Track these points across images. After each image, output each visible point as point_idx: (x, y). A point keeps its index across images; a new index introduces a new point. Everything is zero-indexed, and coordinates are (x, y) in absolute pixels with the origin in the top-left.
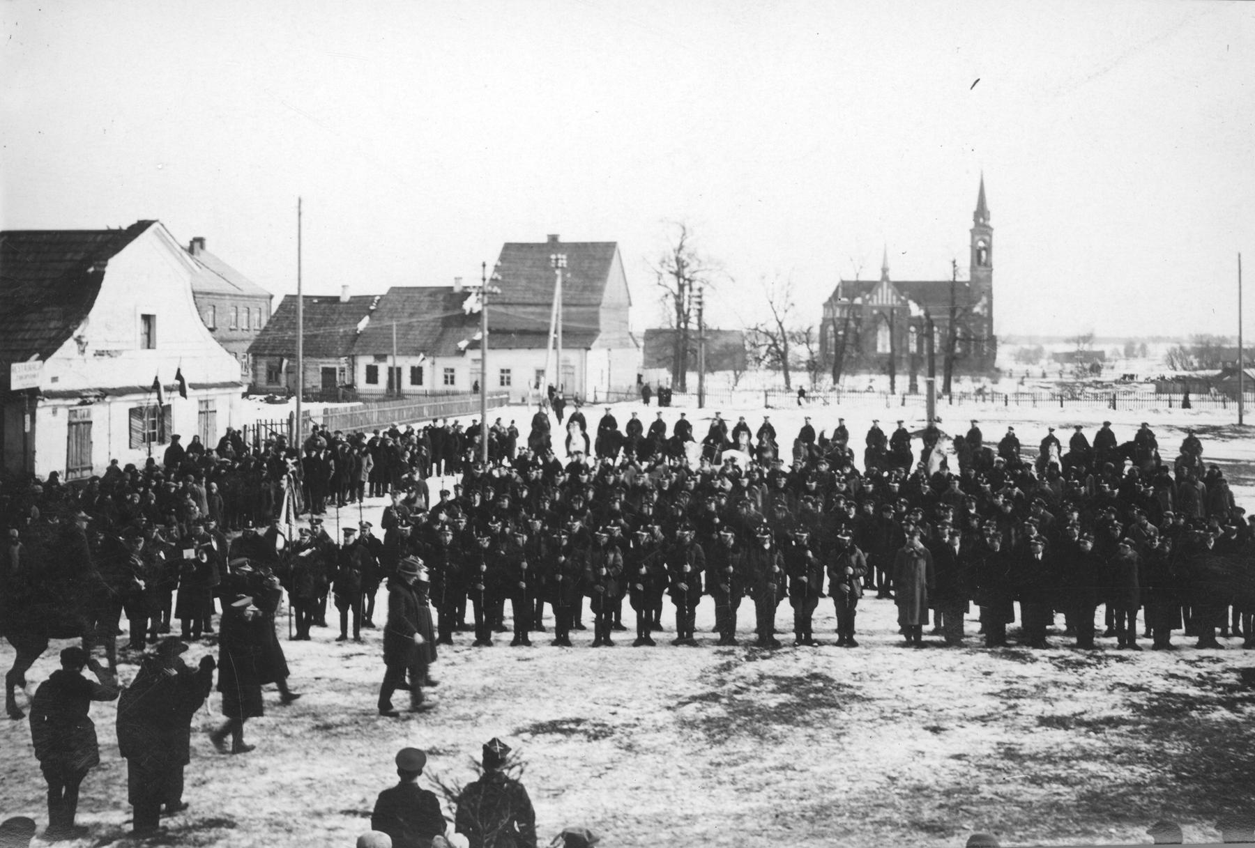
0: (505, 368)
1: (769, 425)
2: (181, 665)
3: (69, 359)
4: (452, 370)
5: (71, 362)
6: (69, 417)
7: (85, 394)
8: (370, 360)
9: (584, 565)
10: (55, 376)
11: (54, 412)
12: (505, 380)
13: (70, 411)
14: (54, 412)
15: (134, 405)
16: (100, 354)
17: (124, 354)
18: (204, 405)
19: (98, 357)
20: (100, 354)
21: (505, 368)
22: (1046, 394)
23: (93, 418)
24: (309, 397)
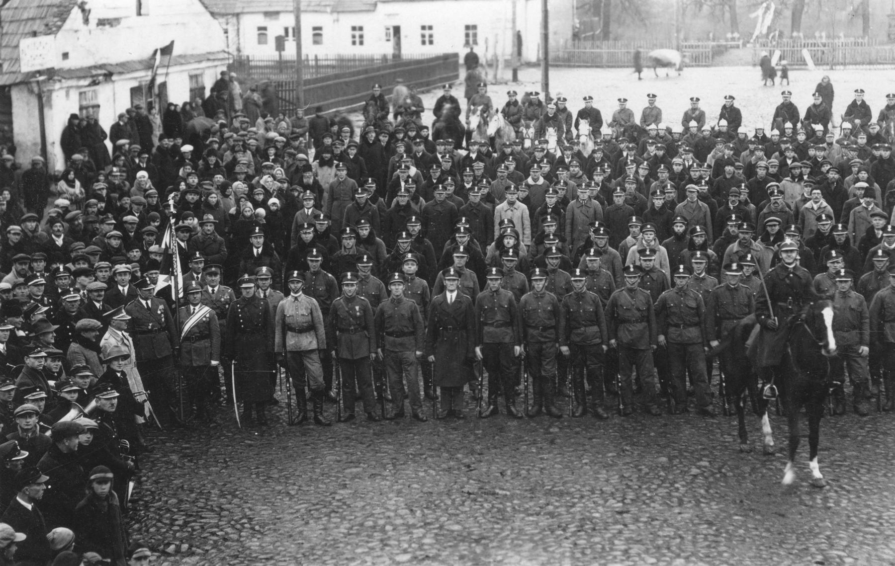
0: (471, 23)
1: (791, 104)
2: (133, 480)
3: (76, 31)
4: (361, 29)
5: (79, 34)
6: (80, 100)
7: (94, 72)
8: (261, 21)
9: (489, 397)
10: (66, 51)
11: (67, 94)
12: (427, 39)
13: (81, 94)
14: (67, 94)
15: (135, 84)
16: (102, 23)
17: (123, 22)
18: (194, 80)
19: (100, 27)
20: (102, 23)
21: (427, 24)
22: (142, 103)
23: (101, 100)
24: (882, 43)
